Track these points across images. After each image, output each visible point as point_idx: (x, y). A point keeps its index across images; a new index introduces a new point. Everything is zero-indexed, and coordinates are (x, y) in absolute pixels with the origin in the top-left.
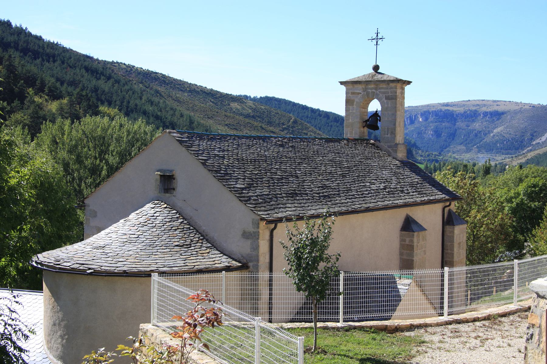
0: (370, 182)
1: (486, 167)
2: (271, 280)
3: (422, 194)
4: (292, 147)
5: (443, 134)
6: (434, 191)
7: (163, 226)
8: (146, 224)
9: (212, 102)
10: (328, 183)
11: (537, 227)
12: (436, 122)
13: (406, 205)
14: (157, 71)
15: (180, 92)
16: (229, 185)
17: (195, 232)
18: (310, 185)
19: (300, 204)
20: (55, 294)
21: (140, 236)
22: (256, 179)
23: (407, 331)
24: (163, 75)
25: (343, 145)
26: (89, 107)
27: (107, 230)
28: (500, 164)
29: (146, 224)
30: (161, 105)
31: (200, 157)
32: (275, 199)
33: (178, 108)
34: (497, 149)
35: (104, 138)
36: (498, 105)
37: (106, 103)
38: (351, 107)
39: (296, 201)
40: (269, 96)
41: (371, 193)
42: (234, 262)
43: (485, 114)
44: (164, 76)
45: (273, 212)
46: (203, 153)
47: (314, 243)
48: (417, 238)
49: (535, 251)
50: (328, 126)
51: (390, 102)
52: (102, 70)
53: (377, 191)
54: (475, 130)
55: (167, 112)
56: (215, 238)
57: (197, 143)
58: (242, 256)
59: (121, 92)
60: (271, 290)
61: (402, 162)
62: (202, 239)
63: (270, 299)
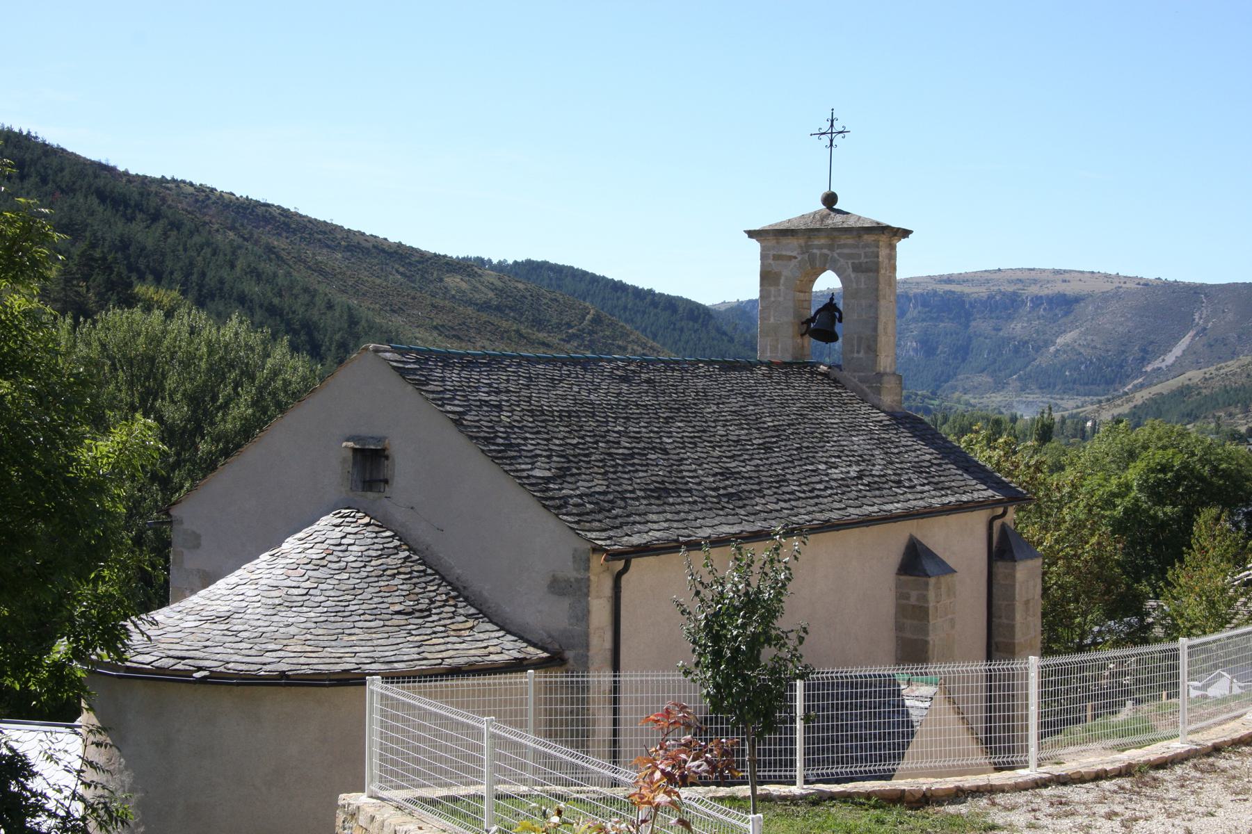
0: (826, 463)
1: (1043, 425)
2: (615, 689)
3: (942, 489)
4: (648, 381)
5: (940, 347)
6: (969, 483)
7: (365, 566)
8: (324, 562)
9: (402, 274)
10: (733, 464)
11: (1177, 565)
12: (924, 320)
13: (909, 515)
14: (269, 202)
15: (325, 251)
16: (517, 471)
17: (437, 582)
18: (695, 471)
19: (678, 513)
20: (111, 730)
21: (311, 592)
22: (574, 456)
23: (952, 803)
24: (283, 210)
25: (760, 377)
26: (111, 286)
27: (232, 579)
28: (1072, 416)
29: (324, 562)
30: (280, 280)
31: (448, 408)
32: (622, 504)
33: (322, 288)
34: (1064, 383)
35: (152, 360)
36: (1064, 281)
37: (150, 278)
38: (772, 289)
39: (667, 508)
40: (534, 258)
41: (832, 488)
42: (531, 649)
43: (1037, 301)
44: (285, 212)
45: (619, 532)
46: (453, 398)
47: (751, 603)
48: (935, 592)
49: (1173, 619)
50: (674, 329)
51: (863, 277)
52: (136, 196)
53: (844, 483)
54: (1014, 338)
55: (296, 297)
56: (486, 594)
57: (438, 373)
58: (550, 636)
59: (185, 250)
60: (615, 712)
61: (892, 415)
62: (454, 598)
63: (615, 733)
